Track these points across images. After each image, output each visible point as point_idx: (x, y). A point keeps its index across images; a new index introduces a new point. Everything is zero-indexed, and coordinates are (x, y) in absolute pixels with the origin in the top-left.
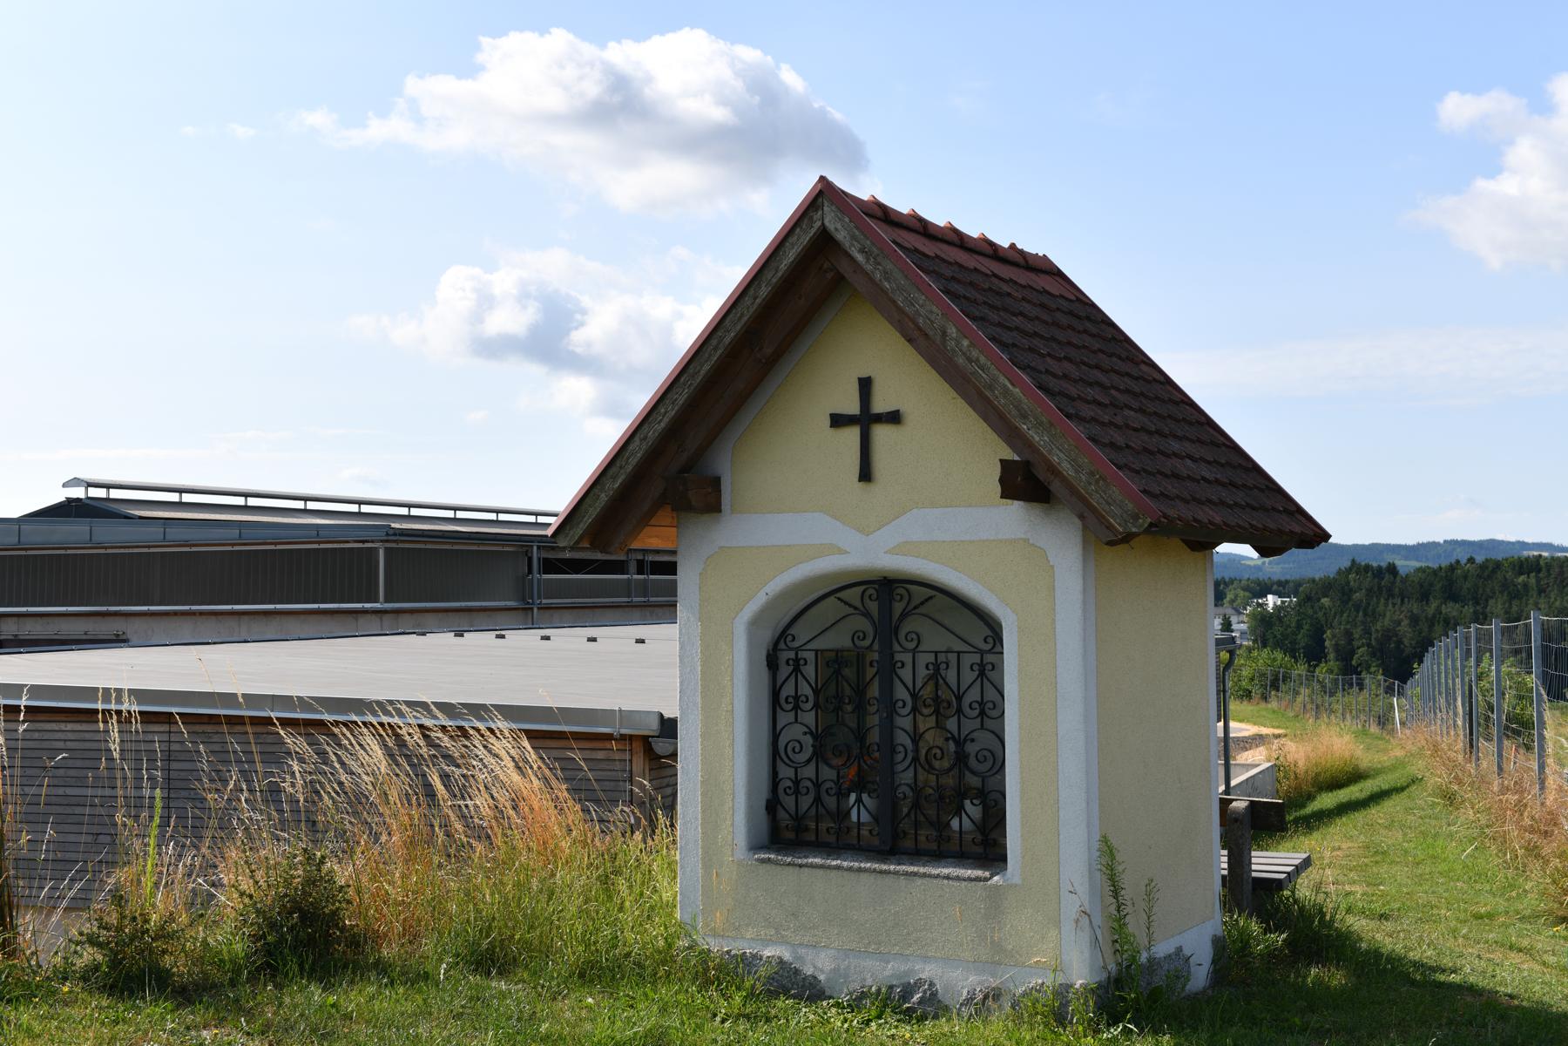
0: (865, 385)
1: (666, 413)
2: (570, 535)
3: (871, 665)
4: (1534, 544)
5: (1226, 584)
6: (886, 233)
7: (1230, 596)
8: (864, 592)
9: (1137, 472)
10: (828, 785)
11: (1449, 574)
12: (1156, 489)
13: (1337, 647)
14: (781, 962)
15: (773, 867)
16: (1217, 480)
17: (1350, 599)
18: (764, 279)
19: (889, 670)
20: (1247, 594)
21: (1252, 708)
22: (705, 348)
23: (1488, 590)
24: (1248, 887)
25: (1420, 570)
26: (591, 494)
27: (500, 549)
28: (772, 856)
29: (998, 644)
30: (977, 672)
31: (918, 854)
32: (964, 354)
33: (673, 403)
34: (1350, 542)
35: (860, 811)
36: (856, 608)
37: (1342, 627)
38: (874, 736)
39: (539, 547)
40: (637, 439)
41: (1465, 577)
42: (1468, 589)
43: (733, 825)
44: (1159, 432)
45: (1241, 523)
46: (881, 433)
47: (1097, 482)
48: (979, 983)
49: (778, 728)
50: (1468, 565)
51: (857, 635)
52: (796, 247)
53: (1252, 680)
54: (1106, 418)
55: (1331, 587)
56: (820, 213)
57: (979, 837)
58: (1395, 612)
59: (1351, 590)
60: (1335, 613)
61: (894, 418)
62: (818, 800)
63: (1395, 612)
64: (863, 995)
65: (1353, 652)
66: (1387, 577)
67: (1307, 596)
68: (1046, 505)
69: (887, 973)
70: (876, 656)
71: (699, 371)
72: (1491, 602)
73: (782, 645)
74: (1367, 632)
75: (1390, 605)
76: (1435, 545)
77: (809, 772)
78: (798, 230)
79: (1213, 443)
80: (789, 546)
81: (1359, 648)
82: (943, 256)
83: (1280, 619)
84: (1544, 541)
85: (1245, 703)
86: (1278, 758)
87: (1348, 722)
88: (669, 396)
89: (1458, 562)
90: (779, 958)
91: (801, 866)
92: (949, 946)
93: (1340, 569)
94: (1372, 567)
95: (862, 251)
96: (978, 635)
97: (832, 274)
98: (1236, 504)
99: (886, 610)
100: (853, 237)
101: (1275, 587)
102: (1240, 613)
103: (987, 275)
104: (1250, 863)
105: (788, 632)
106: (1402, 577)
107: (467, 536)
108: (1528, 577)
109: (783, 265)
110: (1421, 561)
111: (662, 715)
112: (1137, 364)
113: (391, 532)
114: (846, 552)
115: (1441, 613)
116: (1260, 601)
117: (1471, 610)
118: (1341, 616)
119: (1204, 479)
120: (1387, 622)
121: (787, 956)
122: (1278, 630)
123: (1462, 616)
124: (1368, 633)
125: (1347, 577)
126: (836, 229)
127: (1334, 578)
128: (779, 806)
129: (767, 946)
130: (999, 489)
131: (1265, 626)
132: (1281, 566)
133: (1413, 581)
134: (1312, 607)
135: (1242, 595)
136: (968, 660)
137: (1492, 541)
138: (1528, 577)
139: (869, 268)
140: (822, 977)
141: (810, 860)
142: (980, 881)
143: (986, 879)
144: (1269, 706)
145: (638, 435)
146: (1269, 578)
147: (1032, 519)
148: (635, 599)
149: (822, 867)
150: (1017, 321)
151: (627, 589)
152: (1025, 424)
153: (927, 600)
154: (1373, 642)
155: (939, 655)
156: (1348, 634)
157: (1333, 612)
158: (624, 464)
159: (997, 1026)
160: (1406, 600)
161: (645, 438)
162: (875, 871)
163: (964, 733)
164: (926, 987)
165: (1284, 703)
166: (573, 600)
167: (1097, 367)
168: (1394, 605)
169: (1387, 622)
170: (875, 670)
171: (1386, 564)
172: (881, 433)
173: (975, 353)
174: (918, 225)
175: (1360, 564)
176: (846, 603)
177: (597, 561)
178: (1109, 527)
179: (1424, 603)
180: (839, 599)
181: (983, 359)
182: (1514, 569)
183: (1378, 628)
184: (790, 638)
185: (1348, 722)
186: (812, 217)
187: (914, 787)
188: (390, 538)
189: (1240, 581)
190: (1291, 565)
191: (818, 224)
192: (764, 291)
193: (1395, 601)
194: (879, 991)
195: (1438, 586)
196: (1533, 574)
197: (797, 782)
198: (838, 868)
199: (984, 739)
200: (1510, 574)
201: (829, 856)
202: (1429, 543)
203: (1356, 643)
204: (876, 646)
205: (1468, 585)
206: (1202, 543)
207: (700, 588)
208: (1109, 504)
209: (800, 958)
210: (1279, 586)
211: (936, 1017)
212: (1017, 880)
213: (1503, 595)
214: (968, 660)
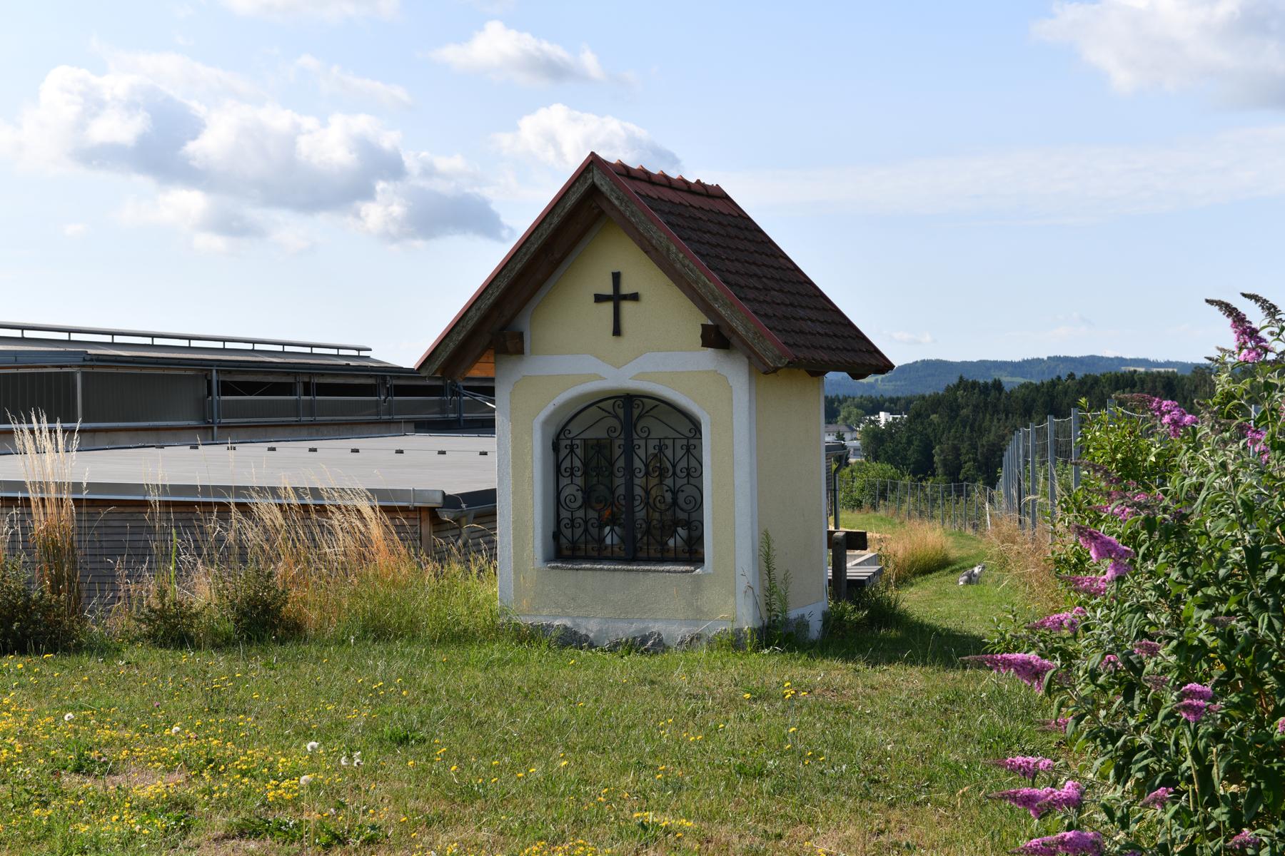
0: (616, 277)
1: (493, 293)
4: (1131, 360)
5: (840, 402)
6: (630, 186)
7: (843, 414)
9: (780, 331)
10: (593, 521)
11: (1050, 390)
12: (791, 342)
13: (945, 463)
14: (566, 628)
16: (826, 334)
19: (629, 450)
20: (860, 411)
21: (862, 516)
24: (844, 585)
26: (443, 344)
27: (183, 373)
28: (559, 565)
29: (698, 434)
31: (649, 560)
32: (680, 262)
35: (610, 537)
36: (609, 413)
37: (950, 442)
38: (621, 491)
39: (217, 371)
40: (474, 309)
41: (1066, 393)
44: (792, 305)
45: (840, 359)
46: (626, 306)
47: (758, 338)
49: (560, 488)
53: (863, 491)
54: (762, 298)
56: (591, 174)
57: (687, 548)
59: (958, 406)
61: (635, 297)
62: (586, 530)
64: (617, 644)
65: (960, 467)
66: (993, 393)
68: (721, 352)
69: (631, 630)
70: (622, 442)
73: (562, 436)
74: (974, 447)
75: (995, 420)
76: (1038, 361)
77: (580, 513)
79: (824, 309)
81: (966, 463)
82: (663, 197)
83: (891, 435)
84: (1141, 356)
85: (856, 512)
86: (880, 549)
87: (947, 525)
88: (495, 282)
89: (1059, 378)
91: (577, 570)
95: (617, 198)
96: (685, 428)
98: (838, 348)
99: (628, 414)
100: (612, 190)
102: (853, 430)
103: (686, 206)
104: (846, 572)
105: (567, 428)
106: (1006, 393)
107: (155, 361)
111: (444, 493)
112: (777, 258)
113: (88, 358)
116: (873, 418)
118: (950, 432)
119: (818, 333)
120: (992, 437)
121: (569, 624)
122: (889, 445)
124: (974, 448)
125: (955, 393)
127: (943, 395)
130: (700, 341)
131: (878, 443)
132: (894, 383)
133: (1017, 397)
134: (922, 423)
136: (679, 443)
137: (1093, 357)
139: (622, 208)
140: (591, 635)
143: (692, 571)
144: (878, 514)
148: (303, 419)
150: (707, 236)
151: (295, 409)
154: (979, 457)
156: (956, 449)
160: (1010, 415)
161: (479, 309)
163: (677, 486)
165: (891, 511)
166: (246, 420)
167: (754, 263)
168: (999, 420)
169: (992, 437)
170: (622, 450)
171: (993, 380)
172: (626, 306)
173: (687, 262)
174: (645, 177)
176: (603, 410)
177: (268, 383)
178: (765, 364)
181: (691, 265)
182: (1110, 385)
183: (984, 443)
185: (947, 525)
186: (586, 177)
187: (648, 521)
188: (88, 363)
189: (854, 398)
191: (590, 181)
192: (556, 220)
193: (1000, 416)
194: (627, 641)
197: (572, 520)
198: (601, 569)
199: (689, 490)
200: (1107, 389)
201: (595, 563)
202: (1033, 360)
203: (963, 458)
204: (622, 436)
206: (817, 371)
209: (578, 625)
211: (663, 651)
212: (710, 571)
214: (679, 443)
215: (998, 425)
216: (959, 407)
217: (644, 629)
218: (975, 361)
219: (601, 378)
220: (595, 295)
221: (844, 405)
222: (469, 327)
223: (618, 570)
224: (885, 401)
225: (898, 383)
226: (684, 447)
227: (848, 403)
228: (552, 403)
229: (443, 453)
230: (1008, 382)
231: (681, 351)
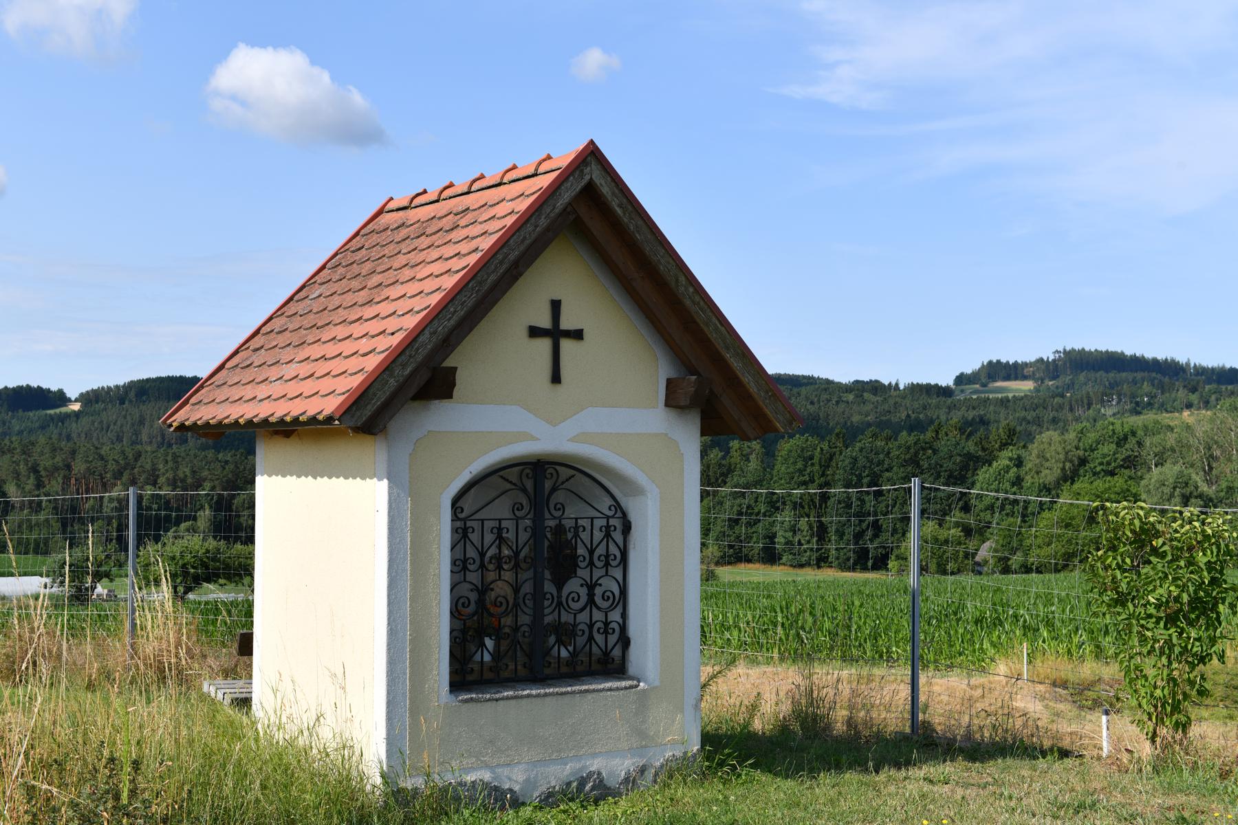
0: (556, 306)
1: (455, 312)
3: (569, 531)
8: (523, 470)
10: (525, 628)
14: (486, 785)
18: (543, 212)
30: (530, 534)
33: (462, 304)
36: (514, 484)
40: (427, 332)
43: (438, 674)
46: (566, 345)
51: (516, 507)
56: (589, 168)
61: (578, 335)
69: (565, 773)
95: (620, 206)
97: (574, 216)
99: (538, 486)
100: (613, 194)
109: (559, 204)
114: (538, 439)
121: (487, 776)
126: (601, 185)
128: (492, 652)
130: (65, 391)
141: (506, 694)
155: (502, 521)
158: (414, 353)
161: (435, 332)
162: (557, 693)
170: (572, 534)
172: (566, 345)
180: (502, 477)
184: (459, 510)
186: (582, 171)
191: (587, 178)
198: (529, 696)
217: (581, 769)
220: (582, 330)
222: (420, 358)
228: (467, 471)
231: (629, 407)
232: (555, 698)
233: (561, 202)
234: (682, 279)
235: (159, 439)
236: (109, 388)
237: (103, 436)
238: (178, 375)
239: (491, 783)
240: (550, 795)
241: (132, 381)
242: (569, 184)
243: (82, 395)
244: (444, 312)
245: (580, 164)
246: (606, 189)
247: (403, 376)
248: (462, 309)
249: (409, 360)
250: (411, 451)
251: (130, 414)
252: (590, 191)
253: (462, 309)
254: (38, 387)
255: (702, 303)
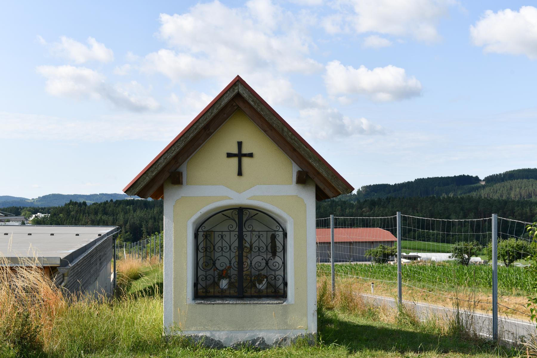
0: (240, 144)
1: (174, 150)
2: (132, 192)
5: (21, 209)
14: (207, 338)
15: (203, 305)
17: (70, 215)
20: (30, 213)
22: (191, 129)
23: (117, 211)
25: (94, 204)
26: (142, 177)
33: (178, 147)
34: (66, 194)
36: (229, 217)
40: (162, 158)
42: (111, 210)
43: (186, 292)
46: (245, 160)
48: (280, 336)
50: (111, 202)
52: (228, 98)
55: (63, 210)
56: (237, 87)
58: (86, 219)
59: (70, 211)
60: (65, 219)
61: (251, 155)
63: (86, 219)
67: (54, 213)
71: (189, 136)
72: (119, 215)
76: (96, 195)
78: (229, 92)
80: (210, 196)
89: (107, 201)
90: (206, 336)
92: (269, 326)
93: (66, 203)
94: (78, 203)
95: (253, 101)
100: (250, 96)
101: (40, 210)
108: (130, 206)
110: (91, 201)
115: (102, 219)
117: (112, 218)
118: (67, 221)
121: (208, 334)
123: (109, 220)
126: (243, 93)
127: (64, 207)
129: (200, 332)
130: (479, 177)
132: (41, 202)
134: (56, 217)
135: (28, 213)
138: (130, 206)
139: (255, 107)
140: (222, 341)
142: (280, 304)
143: (282, 303)
145: (163, 157)
146: (38, 207)
147: (299, 189)
149: (222, 304)
152: (310, 160)
153: (256, 215)
157: (64, 219)
158: (157, 167)
159: (285, 349)
161: (166, 158)
164: (261, 339)
168: (86, 216)
172: (245, 160)
175: (73, 202)
176: (225, 216)
179: (96, 215)
180: (223, 214)
186: (234, 88)
189: (27, 208)
190: (45, 202)
191: (236, 91)
192: (215, 111)
195: (100, 210)
196: (131, 206)
204: (237, 230)
205: (111, 209)
207: (173, 211)
208: (338, 186)
209: (213, 335)
210: (42, 210)
213: (122, 213)
215: (85, 218)
216: (70, 212)
218: (73, 194)
219: (230, 198)
220: (227, 153)
221: (23, 210)
222: (159, 169)
223: (239, 304)
224: (40, 209)
225: (43, 202)
226: (220, 236)
227: (25, 209)
229: (30, 234)
230: (89, 203)
231: (277, 185)
232: (241, 305)
233: (223, 102)
234: (285, 129)
235: (519, 196)
236: (497, 175)
237: (495, 195)
238: (527, 168)
239: (210, 337)
240: (239, 345)
241: (507, 172)
242: (228, 94)
243: (486, 178)
244: (170, 150)
245: (233, 85)
246: (245, 95)
247: (152, 176)
248: (178, 149)
249: (154, 170)
250: (174, 204)
251: (506, 186)
252: (238, 96)
253: (178, 149)
254: (468, 175)
255: (296, 139)
